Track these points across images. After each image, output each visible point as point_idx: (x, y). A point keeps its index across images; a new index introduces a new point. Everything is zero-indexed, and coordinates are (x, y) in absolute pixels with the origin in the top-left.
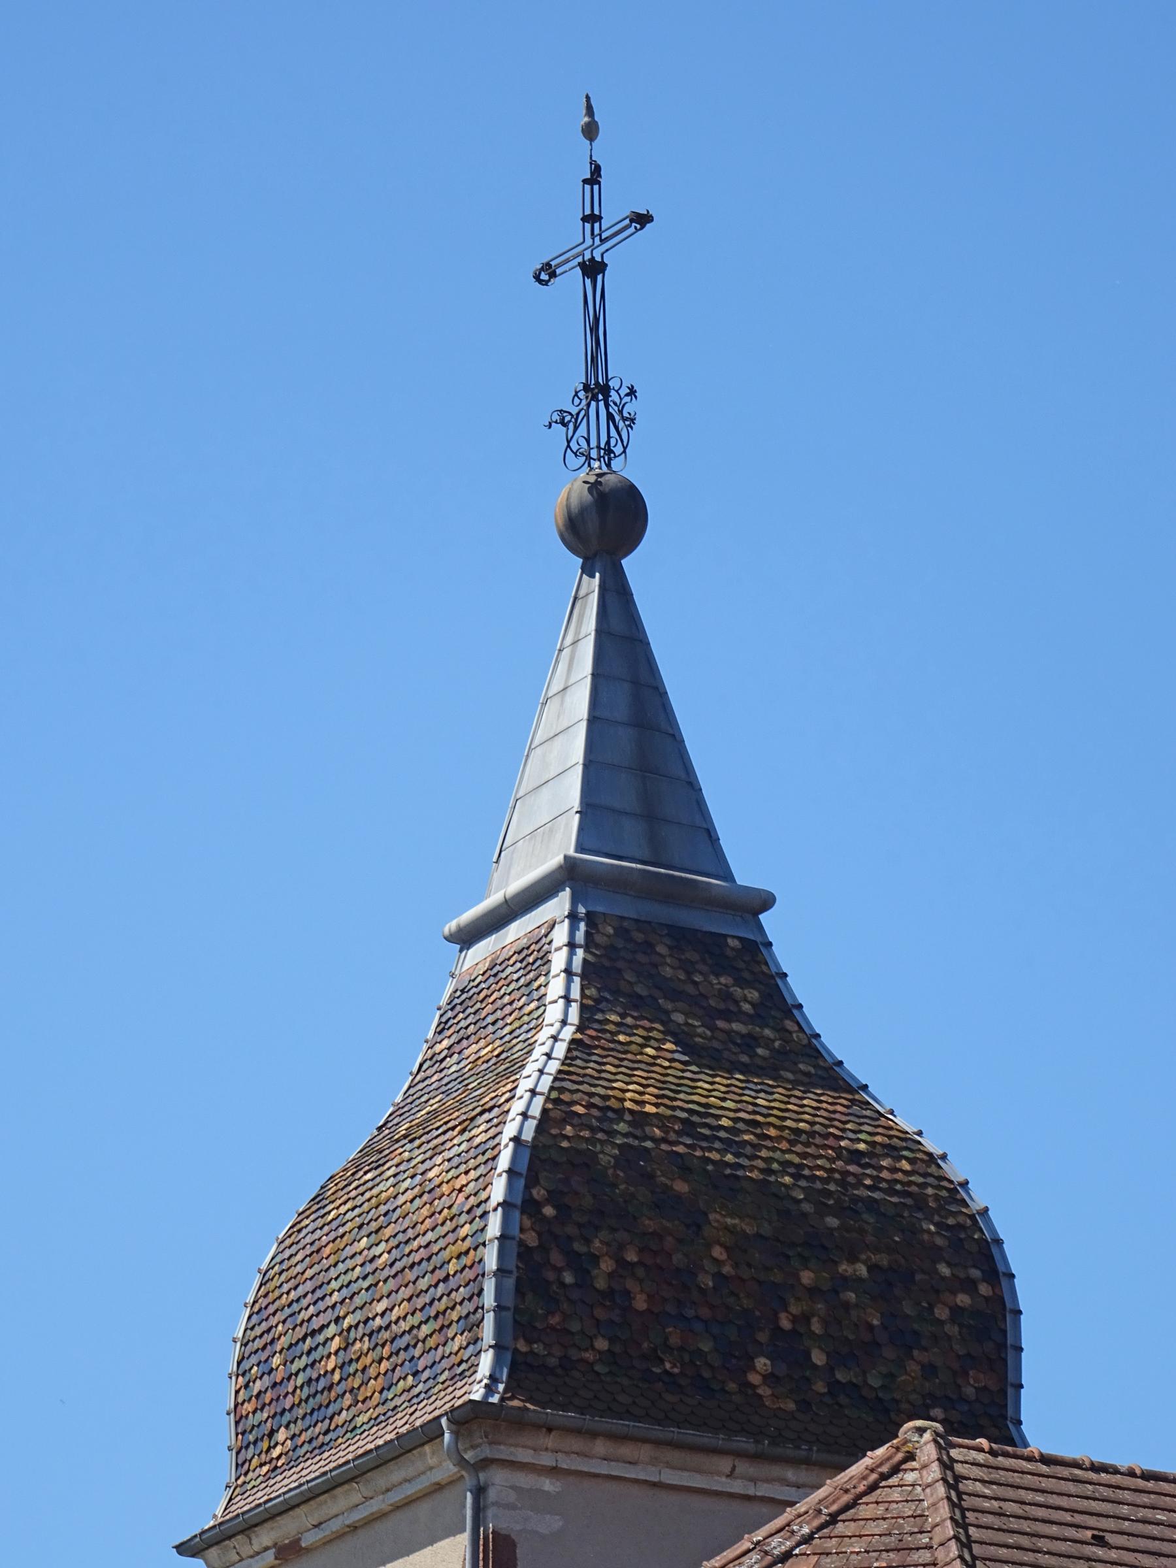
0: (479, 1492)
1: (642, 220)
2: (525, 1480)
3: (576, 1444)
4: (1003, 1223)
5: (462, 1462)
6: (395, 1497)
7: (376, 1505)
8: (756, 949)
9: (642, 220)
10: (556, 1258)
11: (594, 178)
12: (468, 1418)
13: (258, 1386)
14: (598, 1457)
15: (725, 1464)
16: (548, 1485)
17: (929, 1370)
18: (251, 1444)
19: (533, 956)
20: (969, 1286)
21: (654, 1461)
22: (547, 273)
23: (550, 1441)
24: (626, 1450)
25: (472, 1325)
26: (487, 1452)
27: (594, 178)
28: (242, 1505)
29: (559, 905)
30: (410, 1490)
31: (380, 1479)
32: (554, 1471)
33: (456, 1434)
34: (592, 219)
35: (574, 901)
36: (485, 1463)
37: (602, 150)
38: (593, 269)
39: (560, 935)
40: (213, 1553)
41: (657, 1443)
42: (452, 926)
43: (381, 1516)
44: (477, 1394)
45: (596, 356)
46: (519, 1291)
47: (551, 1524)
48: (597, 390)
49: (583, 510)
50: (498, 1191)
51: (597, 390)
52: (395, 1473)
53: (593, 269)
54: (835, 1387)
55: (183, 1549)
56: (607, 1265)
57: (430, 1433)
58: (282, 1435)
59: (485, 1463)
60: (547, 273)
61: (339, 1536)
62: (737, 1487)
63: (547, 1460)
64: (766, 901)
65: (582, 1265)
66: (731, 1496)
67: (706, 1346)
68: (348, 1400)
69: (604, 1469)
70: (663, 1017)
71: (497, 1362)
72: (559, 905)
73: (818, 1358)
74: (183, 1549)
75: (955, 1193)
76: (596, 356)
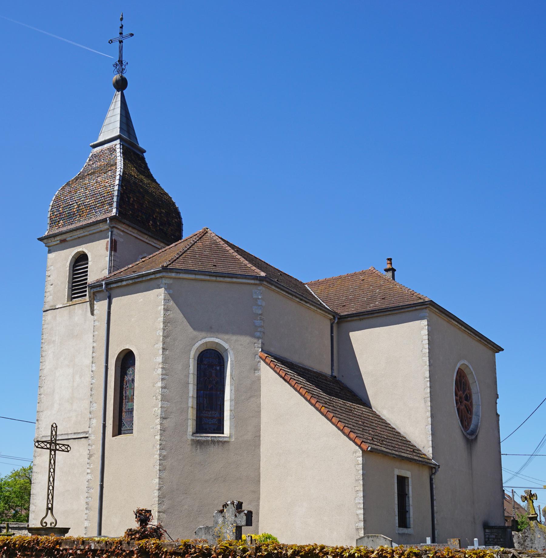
0: (112, 232)
1: (132, 35)
2: (119, 232)
3: (127, 227)
4: (180, 210)
5: (110, 226)
6: (91, 232)
7: (86, 234)
8: (143, 159)
9: (132, 35)
10: (125, 196)
11: (121, 27)
12: (112, 219)
13: (56, 213)
14: (129, 230)
15: (146, 237)
16: (122, 233)
17: (172, 230)
18: (53, 222)
19: (112, 150)
20: (177, 218)
21: (137, 234)
22: (111, 42)
23: (124, 226)
24: (134, 231)
25: (111, 205)
26: (114, 225)
27: (121, 27)
28: (51, 233)
29: (118, 141)
30: (94, 231)
31: (88, 229)
32: (123, 231)
33: (110, 221)
34: (121, 34)
35: (120, 141)
36: (114, 227)
37: (123, 22)
38: (121, 42)
39: (118, 146)
40: (45, 241)
41: (138, 230)
42: (92, 144)
43: (86, 236)
44: (113, 215)
45: (121, 56)
46: (120, 200)
47: (122, 240)
48: (121, 61)
49: (119, 80)
50: (117, 182)
51: (121, 61)
52: (92, 228)
53: (121, 42)
54: (160, 228)
55: (38, 239)
56: (132, 199)
57: (105, 220)
58: (61, 222)
59: (114, 227)
60: (111, 42)
61: (75, 239)
62: (147, 241)
63: (122, 229)
64: (145, 152)
65: (129, 198)
66: (145, 242)
67: (144, 217)
68: (78, 216)
69: (130, 233)
70: (133, 164)
71: (117, 210)
72: (118, 141)
73: (158, 224)
74: (38, 239)
75: (174, 204)
76: (121, 56)
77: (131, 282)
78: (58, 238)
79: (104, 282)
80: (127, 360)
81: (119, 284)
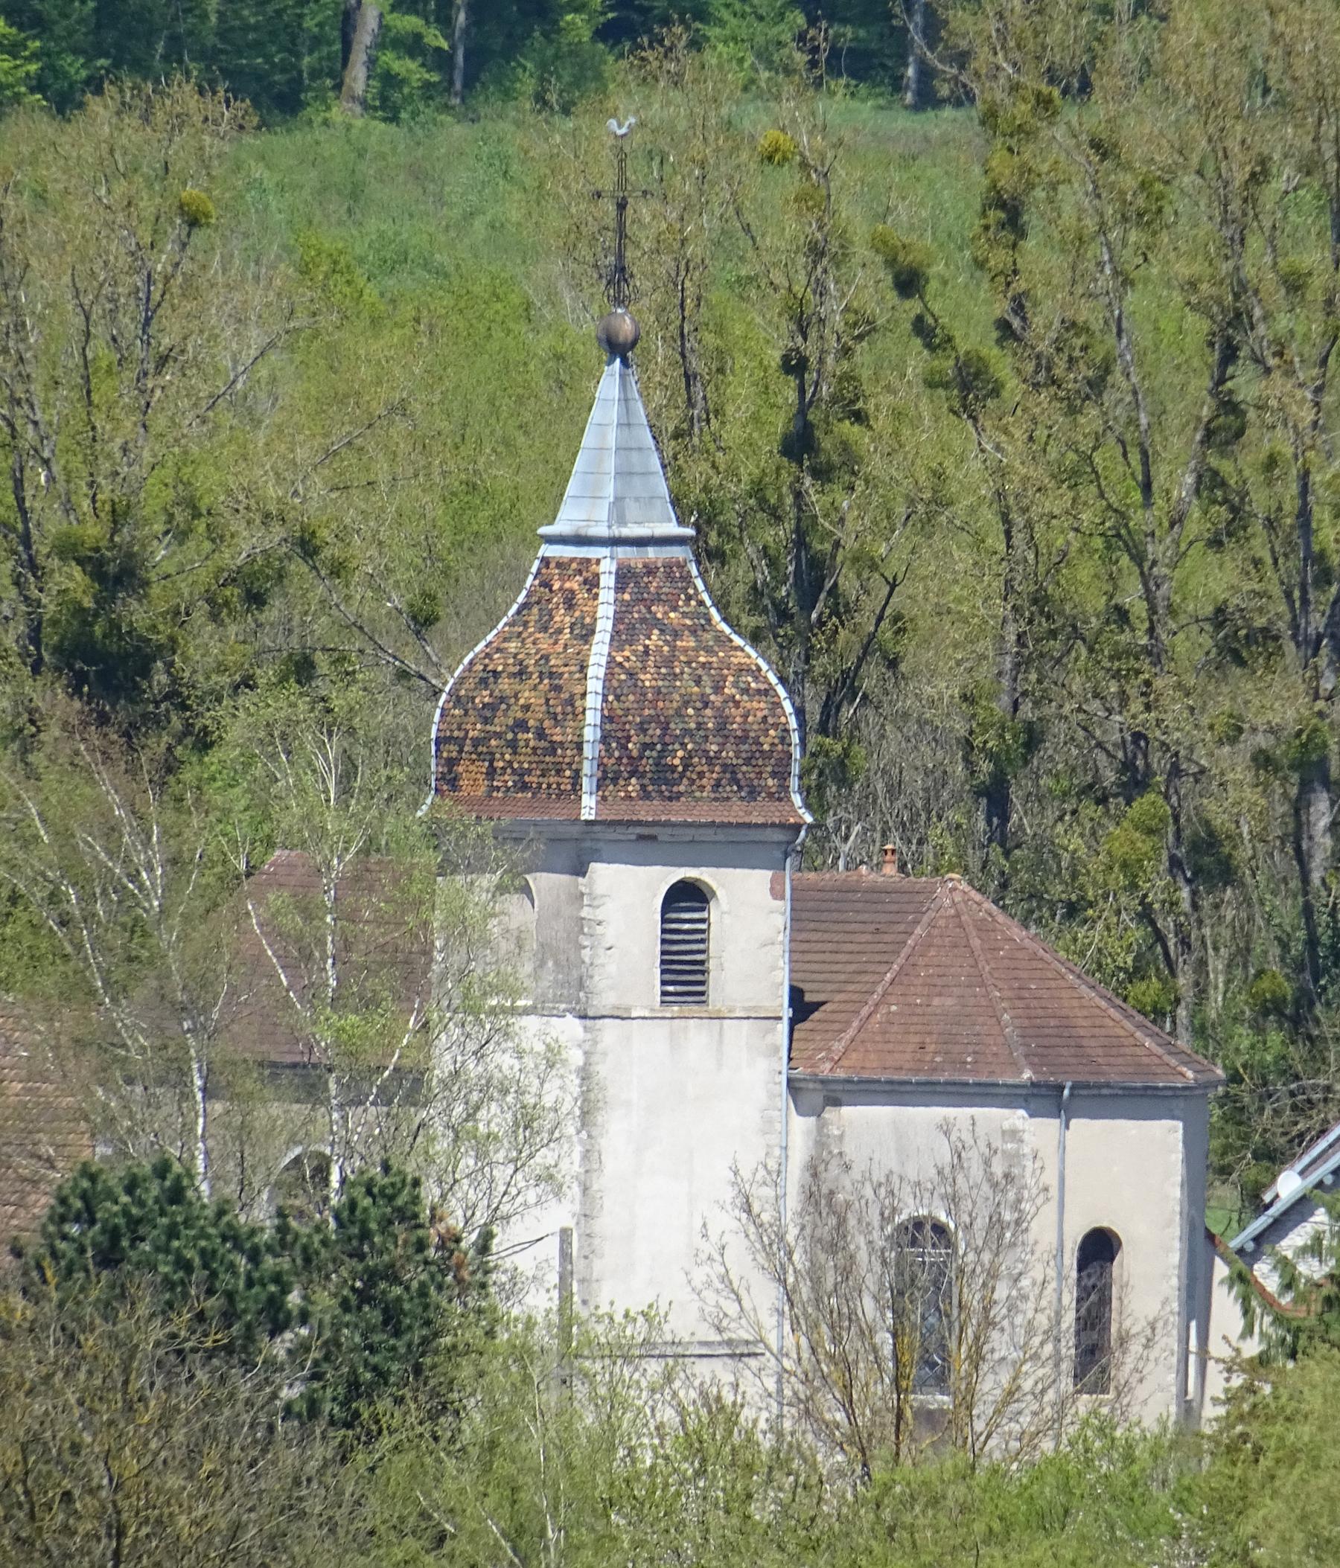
78: (639, 830)
79: (1069, 1084)
80: (1099, 1247)
81: (1095, 1092)
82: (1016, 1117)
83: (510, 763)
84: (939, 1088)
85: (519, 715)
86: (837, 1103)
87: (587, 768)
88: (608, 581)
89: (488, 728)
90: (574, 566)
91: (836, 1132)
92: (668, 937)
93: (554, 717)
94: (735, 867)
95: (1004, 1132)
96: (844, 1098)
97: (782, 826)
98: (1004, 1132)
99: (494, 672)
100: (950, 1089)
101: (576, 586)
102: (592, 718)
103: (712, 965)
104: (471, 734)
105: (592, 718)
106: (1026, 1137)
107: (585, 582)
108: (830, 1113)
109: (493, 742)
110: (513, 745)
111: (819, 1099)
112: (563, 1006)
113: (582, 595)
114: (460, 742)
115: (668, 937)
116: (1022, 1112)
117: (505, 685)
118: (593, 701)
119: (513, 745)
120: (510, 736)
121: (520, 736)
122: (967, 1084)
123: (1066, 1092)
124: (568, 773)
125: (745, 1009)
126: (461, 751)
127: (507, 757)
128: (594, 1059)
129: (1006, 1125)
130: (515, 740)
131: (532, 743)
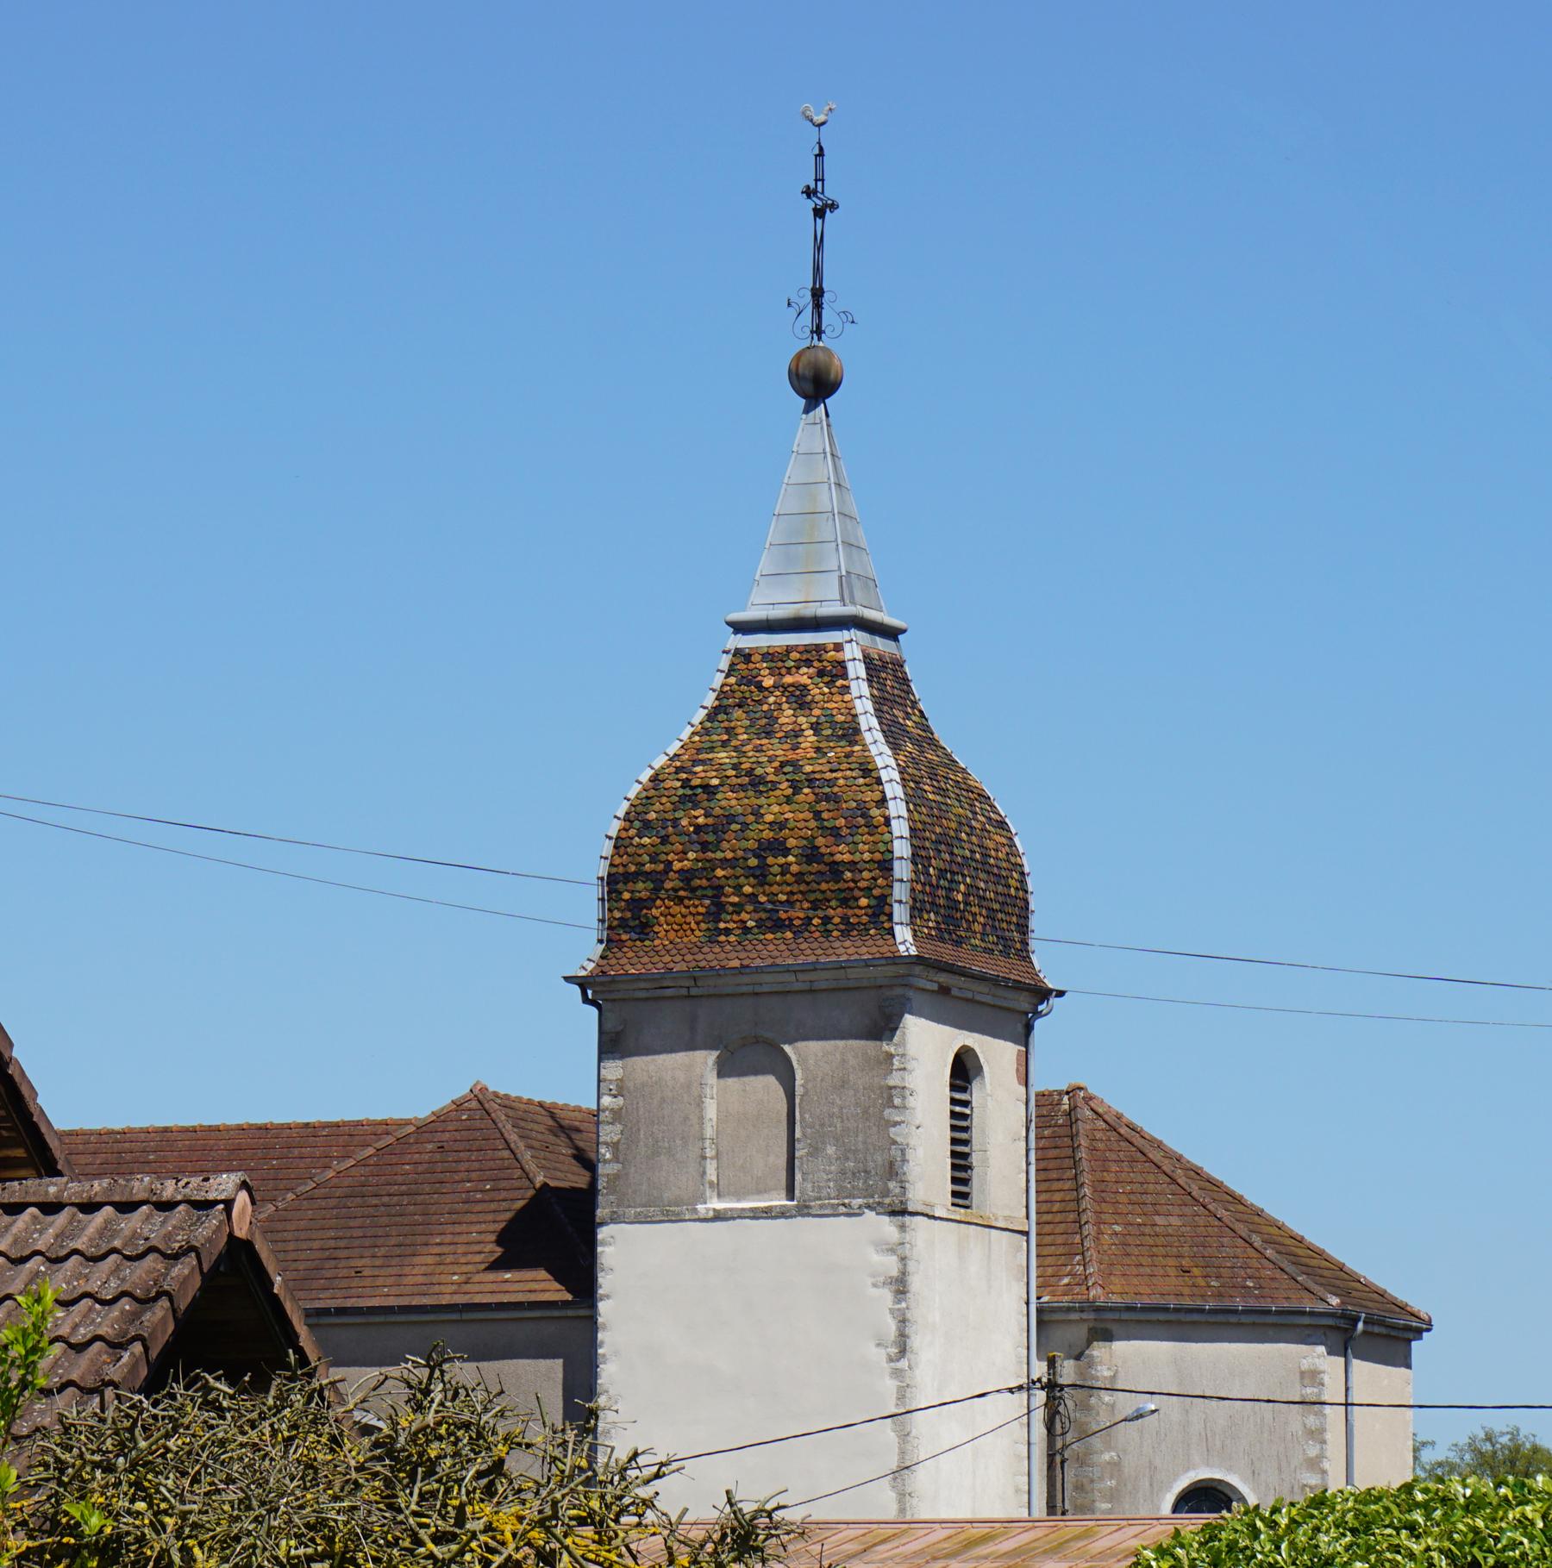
6: (999, 1003)
77: (1383, 1330)
82: (1316, 1356)
83: (752, 897)
84: (1233, 1319)
85: (768, 834)
86: (1108, 1337)
87: (900, 892)
88: (857, 670)
89: (710, 855)
90: (795, 655)
91: (1107, 1373)
92: (958, 1109)
93: (835, 833)
94: (995, 1036)
95: (1302, 1374)
96: (1114, 1328)
97: (1018, 986)
98: (1302, 1374)
99: (706, 787)
100: (1220, 1318)
101: (805, 680)
102: (900, 828)
103: (975, 1182)
104: (677, 866)
105: (900, 828)
106: (1326, 1379)
107: (821, 673)
108: (1099, 1351)
109: (720, 873)
110: (761, 875)
111: (1082, 1332)
112: (857, 1202)
113: (818, 691)
114: (657, 879)
115: (958, 1109)
116: (1321, 1349)
117: (729, 800)
118: (897, 808)
119: (761, 875)
120: (753, 862)
121: (770, 860)
122: (1268, 1312)
123: (1360, 1326)
124: (864, 902)
125: (1006, 1218)
126: (657, 890)
127: (747, 889)
128: (911, 1266)
129: (1306, 1364)
130: (763, 866)
131: (794, 868)
